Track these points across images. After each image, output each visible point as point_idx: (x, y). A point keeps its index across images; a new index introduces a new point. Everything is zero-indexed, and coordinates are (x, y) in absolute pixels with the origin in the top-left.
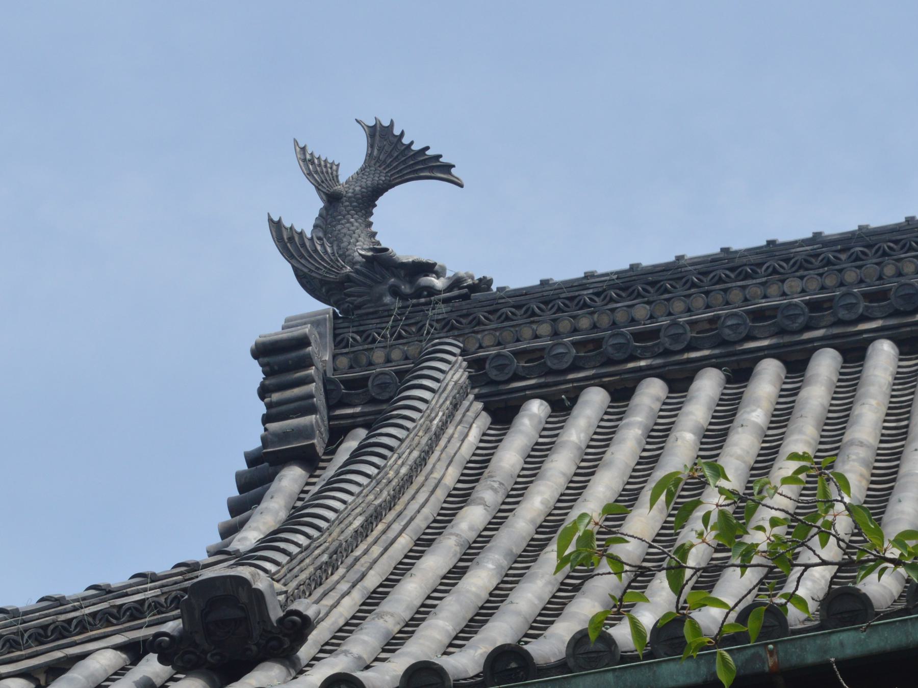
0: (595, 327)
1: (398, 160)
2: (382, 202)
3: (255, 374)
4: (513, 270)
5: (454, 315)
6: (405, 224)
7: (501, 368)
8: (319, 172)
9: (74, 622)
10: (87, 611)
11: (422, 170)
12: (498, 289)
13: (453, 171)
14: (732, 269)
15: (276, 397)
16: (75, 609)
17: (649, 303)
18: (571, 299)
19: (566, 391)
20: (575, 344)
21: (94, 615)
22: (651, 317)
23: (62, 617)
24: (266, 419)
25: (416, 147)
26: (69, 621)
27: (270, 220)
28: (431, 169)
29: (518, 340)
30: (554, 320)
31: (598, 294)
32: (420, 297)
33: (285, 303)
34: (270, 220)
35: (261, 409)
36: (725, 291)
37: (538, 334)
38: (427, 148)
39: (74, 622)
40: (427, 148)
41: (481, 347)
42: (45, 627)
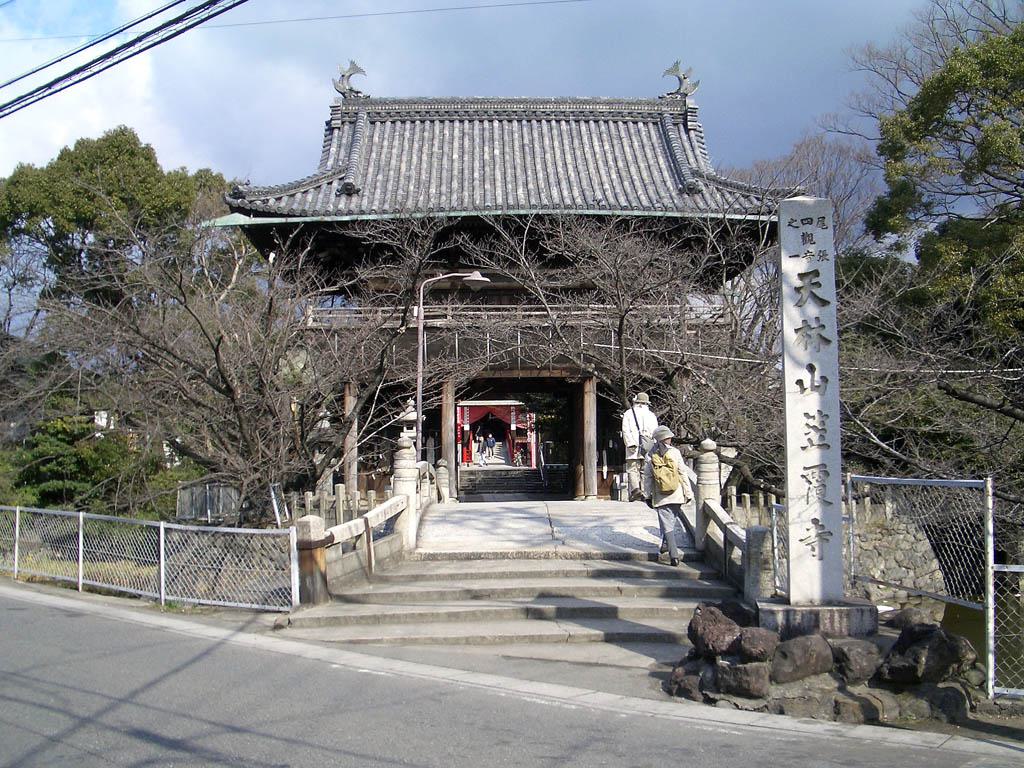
6: (356, 82)
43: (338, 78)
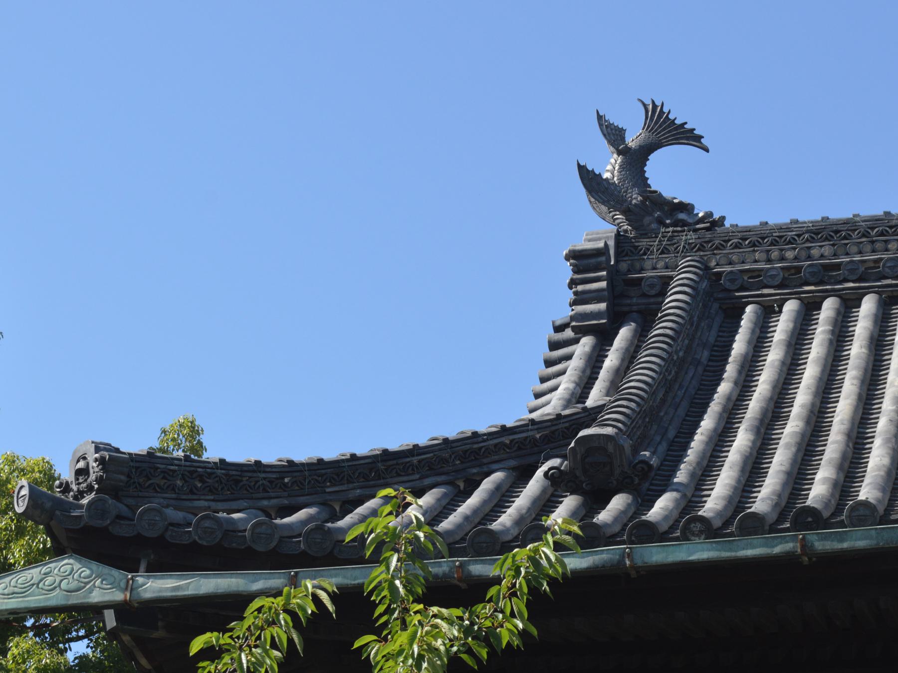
0: (796, 258)
1: (667, 131)
2: (652, 157)
3: (566, 271)
4: (740, 214)
5: (700, 241)
6: (671, 174)
7: (732, 281)
8: (614, 135)
9: (483, 450)
10: (491, 442)
11: (682, 138)
12: (732, 226)
13: (702, 140)
14: (891, 227)
15: (580, 288)
16: (484, 441)
17: (833, 245)
18: (780, 237)
19: (775, 300)
20: (782, 268)
21: (496, 445)
22: (835, 255)
23: (476, 446)
24: (574, 303)
25: (678, 122)
26: (480, 448)
27: (579, 164)
28: (687, 138)
29: (743, 262)
30: (768, 251)
31: (799, 236)
32: (676, 226)
33: (596, 229)
34: (579, 164)
35: (570, 295)
36: (886, 242)
37: (756, 262)
38: (686, 123)
39: (483, 450)
40: (686, 123)
41: (718, 265)
42: (465, 452)
43: (609, 167)
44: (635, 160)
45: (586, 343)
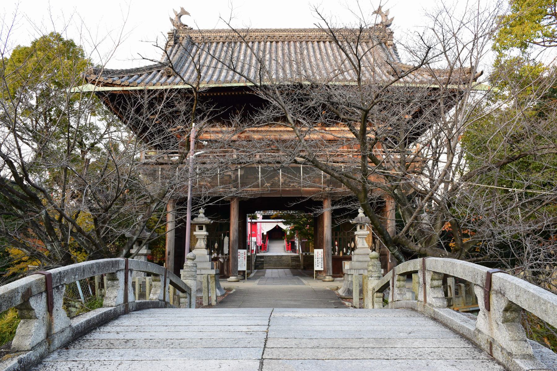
1: (184, 12)
6: (185, 20)
43: (174, 17)
44: (179, 16)
45: (170, 48)
